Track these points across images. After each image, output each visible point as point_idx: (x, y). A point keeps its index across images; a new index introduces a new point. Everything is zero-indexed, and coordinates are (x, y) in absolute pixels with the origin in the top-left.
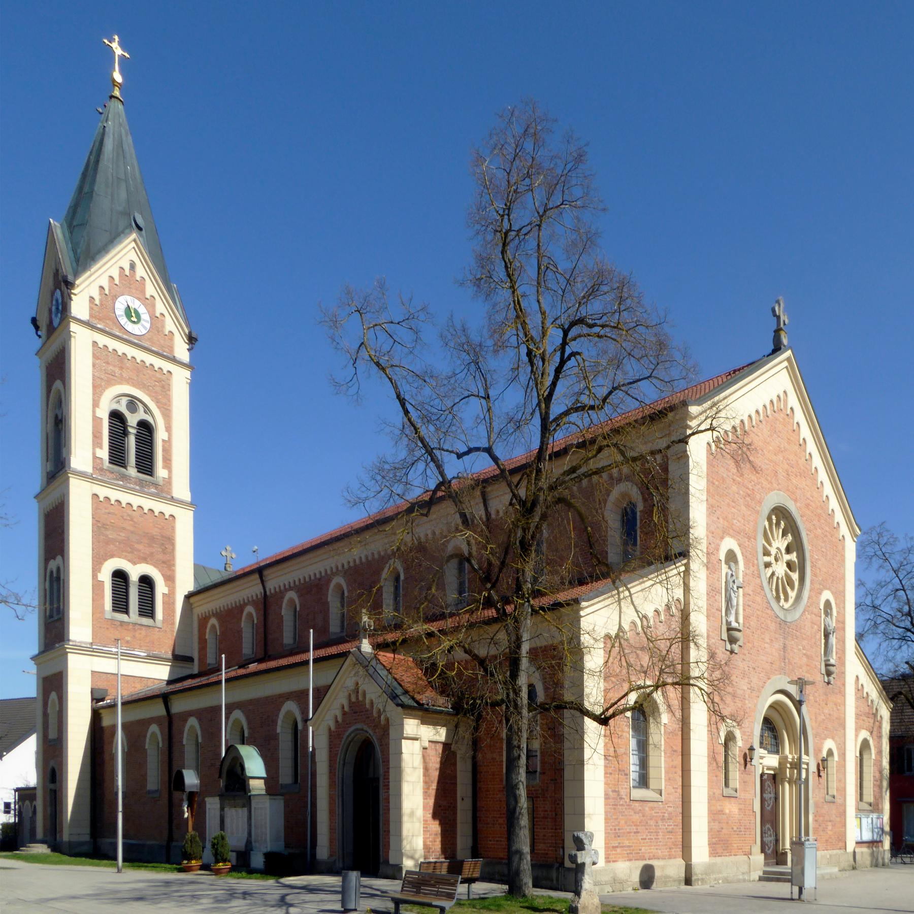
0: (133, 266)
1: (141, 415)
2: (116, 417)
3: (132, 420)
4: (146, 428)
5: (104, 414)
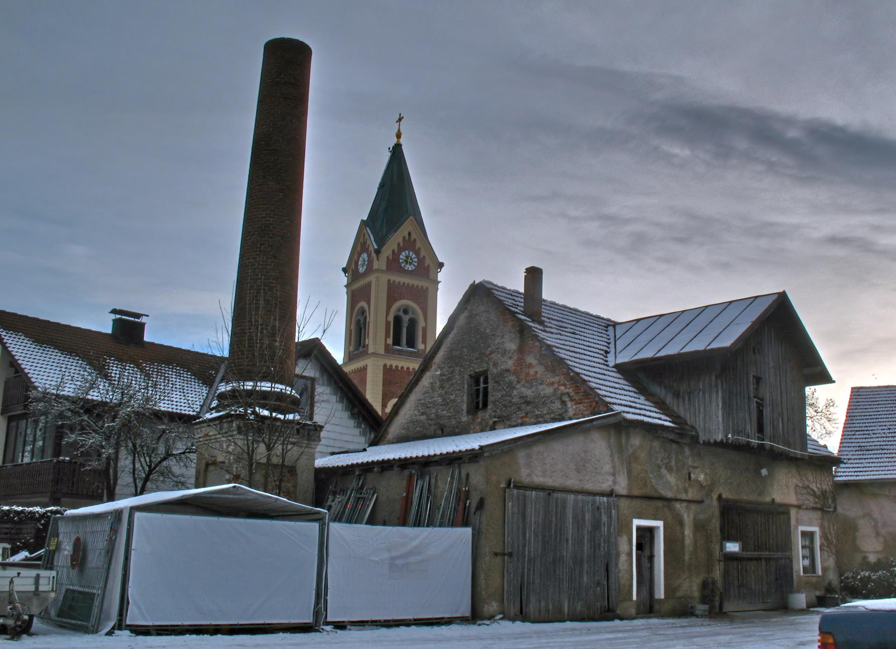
0: (410, 234)
1: (410, 316)
2: (398, 320)
3: (406, 319)
4: (413, 323)
5: (391, 318)
